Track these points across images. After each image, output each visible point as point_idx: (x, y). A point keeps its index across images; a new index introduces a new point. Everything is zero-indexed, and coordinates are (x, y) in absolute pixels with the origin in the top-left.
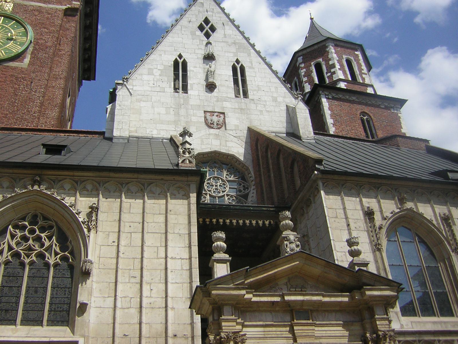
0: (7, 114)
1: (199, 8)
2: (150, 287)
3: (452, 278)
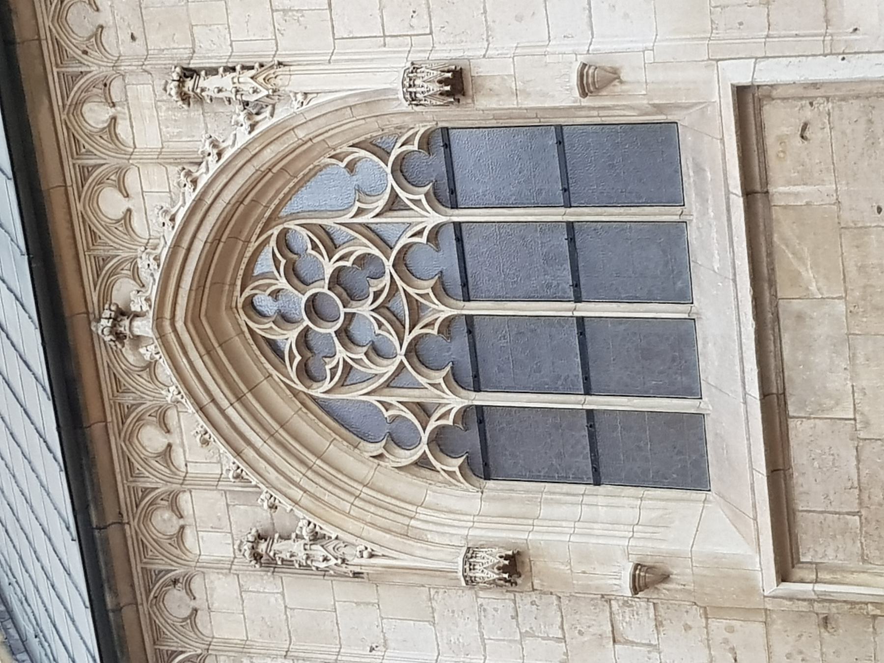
3: (247, 357)
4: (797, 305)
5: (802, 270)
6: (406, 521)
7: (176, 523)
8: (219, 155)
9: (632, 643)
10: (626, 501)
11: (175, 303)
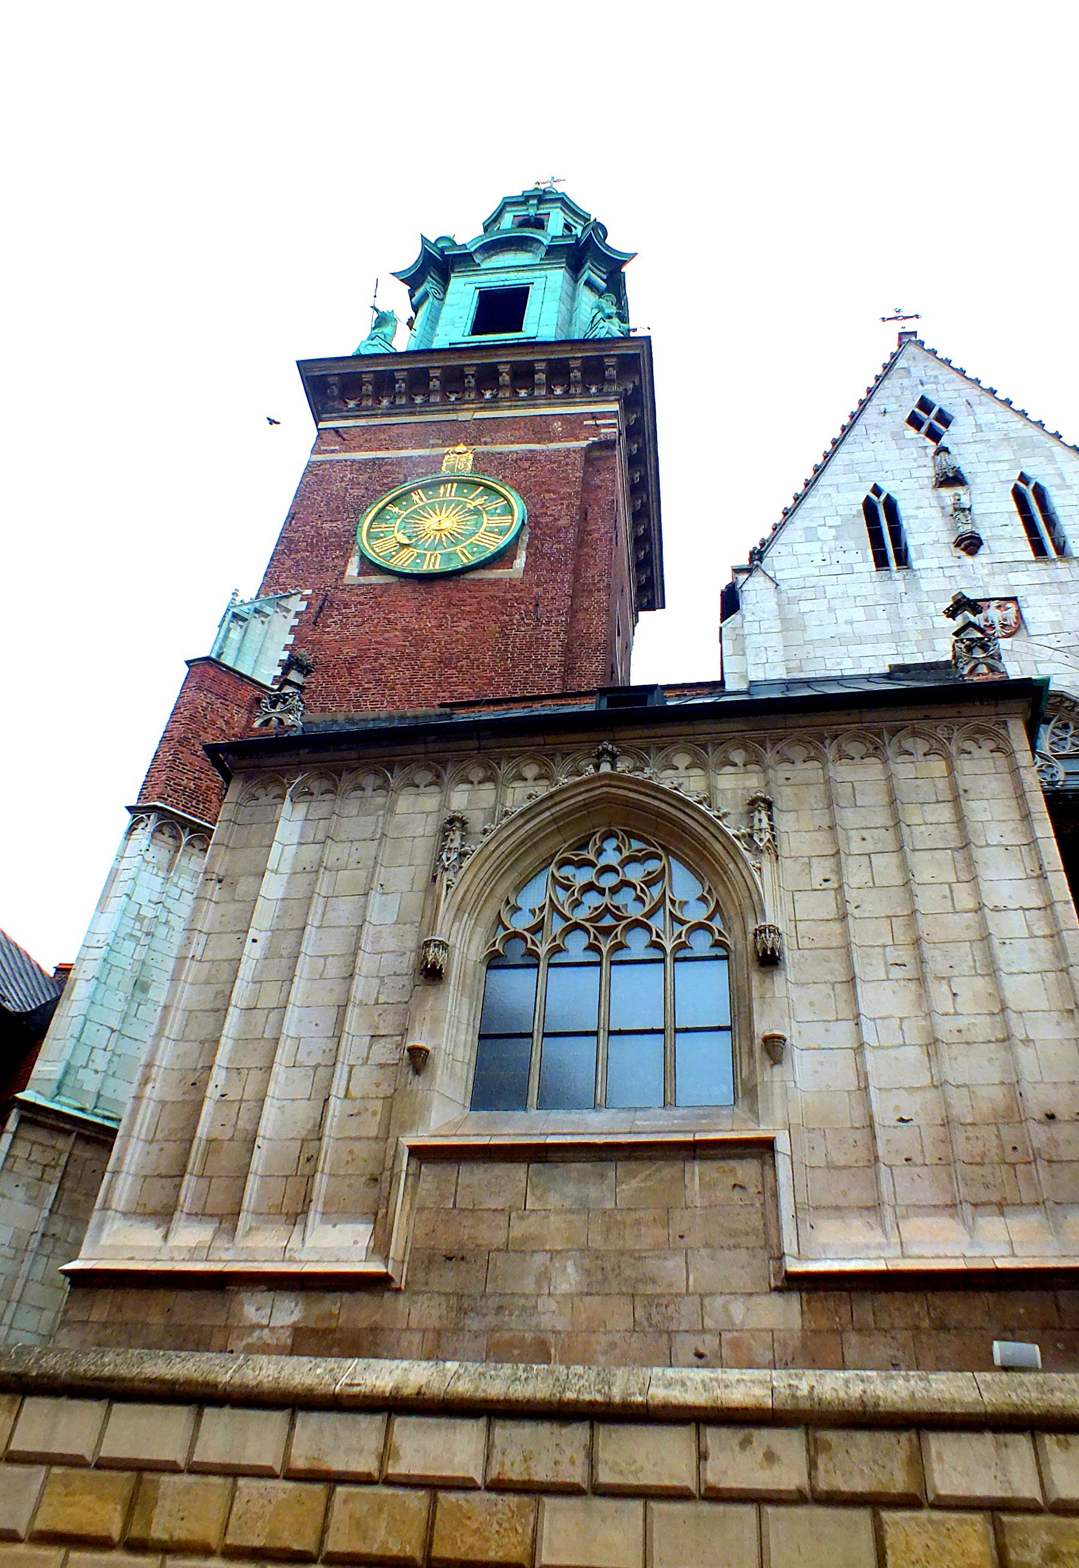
0: (492, 678)
1: (901, 381)
2: (950, 987)
4: (612, 1174)
5: (637, 1179)
6: (468, 911)
7: (476, 780)
8: (718, 817)
9: (370, 1047)
10: (468, 1054)
11: (619, 787)
